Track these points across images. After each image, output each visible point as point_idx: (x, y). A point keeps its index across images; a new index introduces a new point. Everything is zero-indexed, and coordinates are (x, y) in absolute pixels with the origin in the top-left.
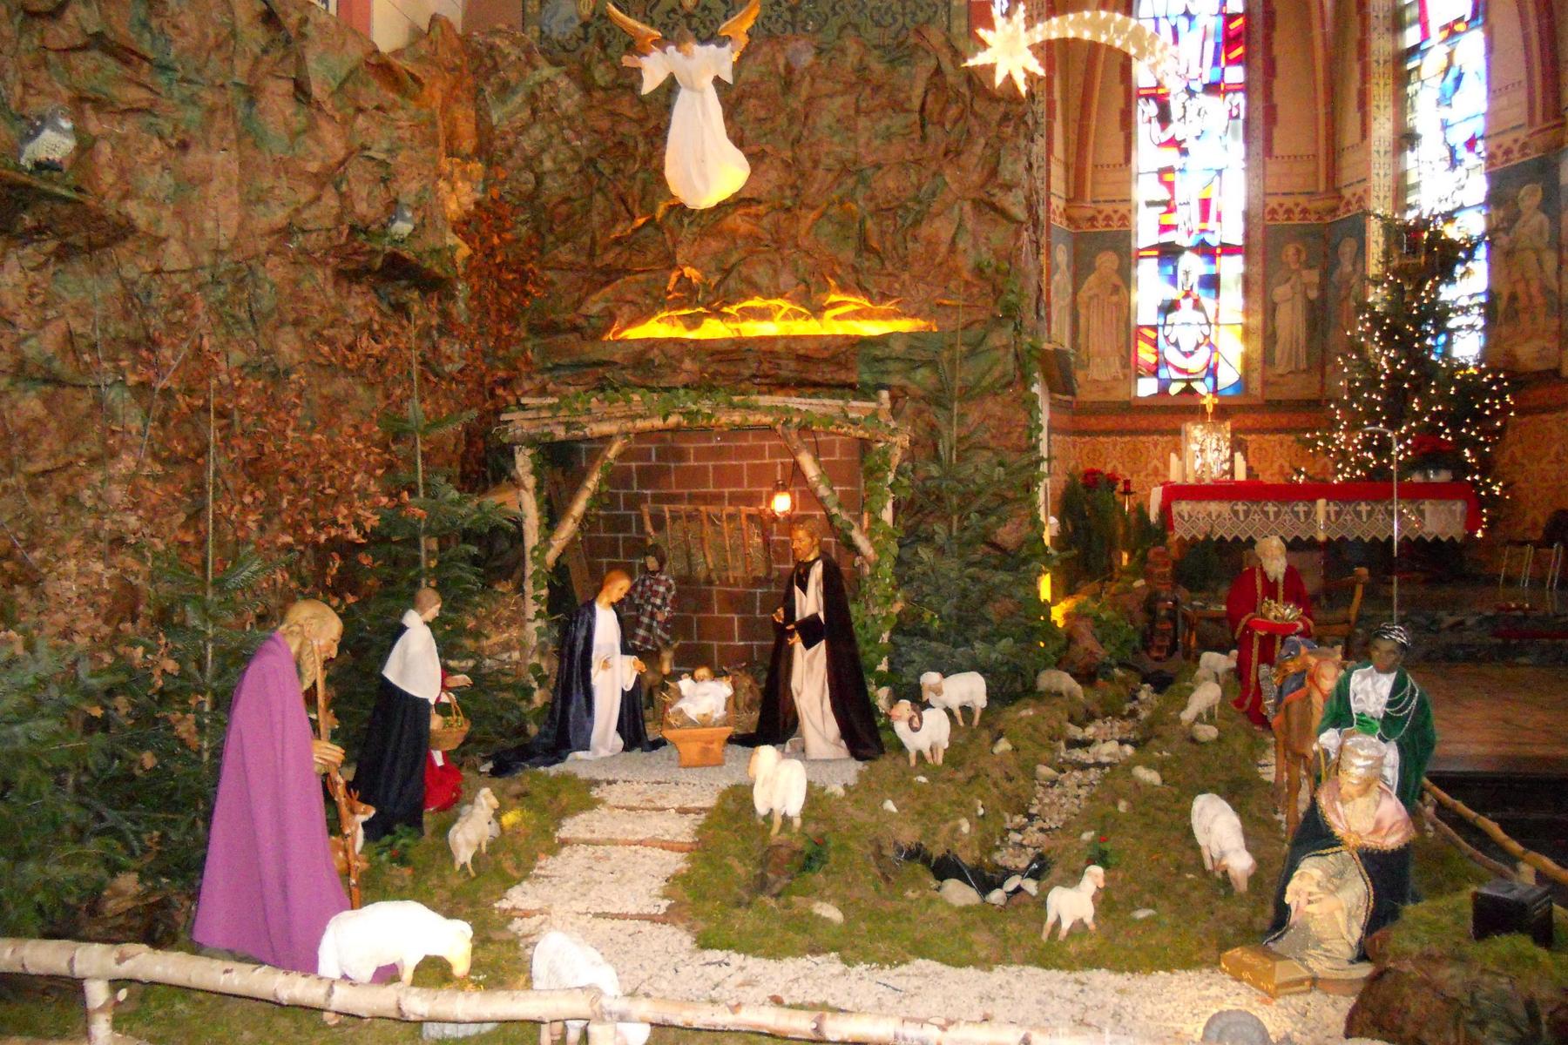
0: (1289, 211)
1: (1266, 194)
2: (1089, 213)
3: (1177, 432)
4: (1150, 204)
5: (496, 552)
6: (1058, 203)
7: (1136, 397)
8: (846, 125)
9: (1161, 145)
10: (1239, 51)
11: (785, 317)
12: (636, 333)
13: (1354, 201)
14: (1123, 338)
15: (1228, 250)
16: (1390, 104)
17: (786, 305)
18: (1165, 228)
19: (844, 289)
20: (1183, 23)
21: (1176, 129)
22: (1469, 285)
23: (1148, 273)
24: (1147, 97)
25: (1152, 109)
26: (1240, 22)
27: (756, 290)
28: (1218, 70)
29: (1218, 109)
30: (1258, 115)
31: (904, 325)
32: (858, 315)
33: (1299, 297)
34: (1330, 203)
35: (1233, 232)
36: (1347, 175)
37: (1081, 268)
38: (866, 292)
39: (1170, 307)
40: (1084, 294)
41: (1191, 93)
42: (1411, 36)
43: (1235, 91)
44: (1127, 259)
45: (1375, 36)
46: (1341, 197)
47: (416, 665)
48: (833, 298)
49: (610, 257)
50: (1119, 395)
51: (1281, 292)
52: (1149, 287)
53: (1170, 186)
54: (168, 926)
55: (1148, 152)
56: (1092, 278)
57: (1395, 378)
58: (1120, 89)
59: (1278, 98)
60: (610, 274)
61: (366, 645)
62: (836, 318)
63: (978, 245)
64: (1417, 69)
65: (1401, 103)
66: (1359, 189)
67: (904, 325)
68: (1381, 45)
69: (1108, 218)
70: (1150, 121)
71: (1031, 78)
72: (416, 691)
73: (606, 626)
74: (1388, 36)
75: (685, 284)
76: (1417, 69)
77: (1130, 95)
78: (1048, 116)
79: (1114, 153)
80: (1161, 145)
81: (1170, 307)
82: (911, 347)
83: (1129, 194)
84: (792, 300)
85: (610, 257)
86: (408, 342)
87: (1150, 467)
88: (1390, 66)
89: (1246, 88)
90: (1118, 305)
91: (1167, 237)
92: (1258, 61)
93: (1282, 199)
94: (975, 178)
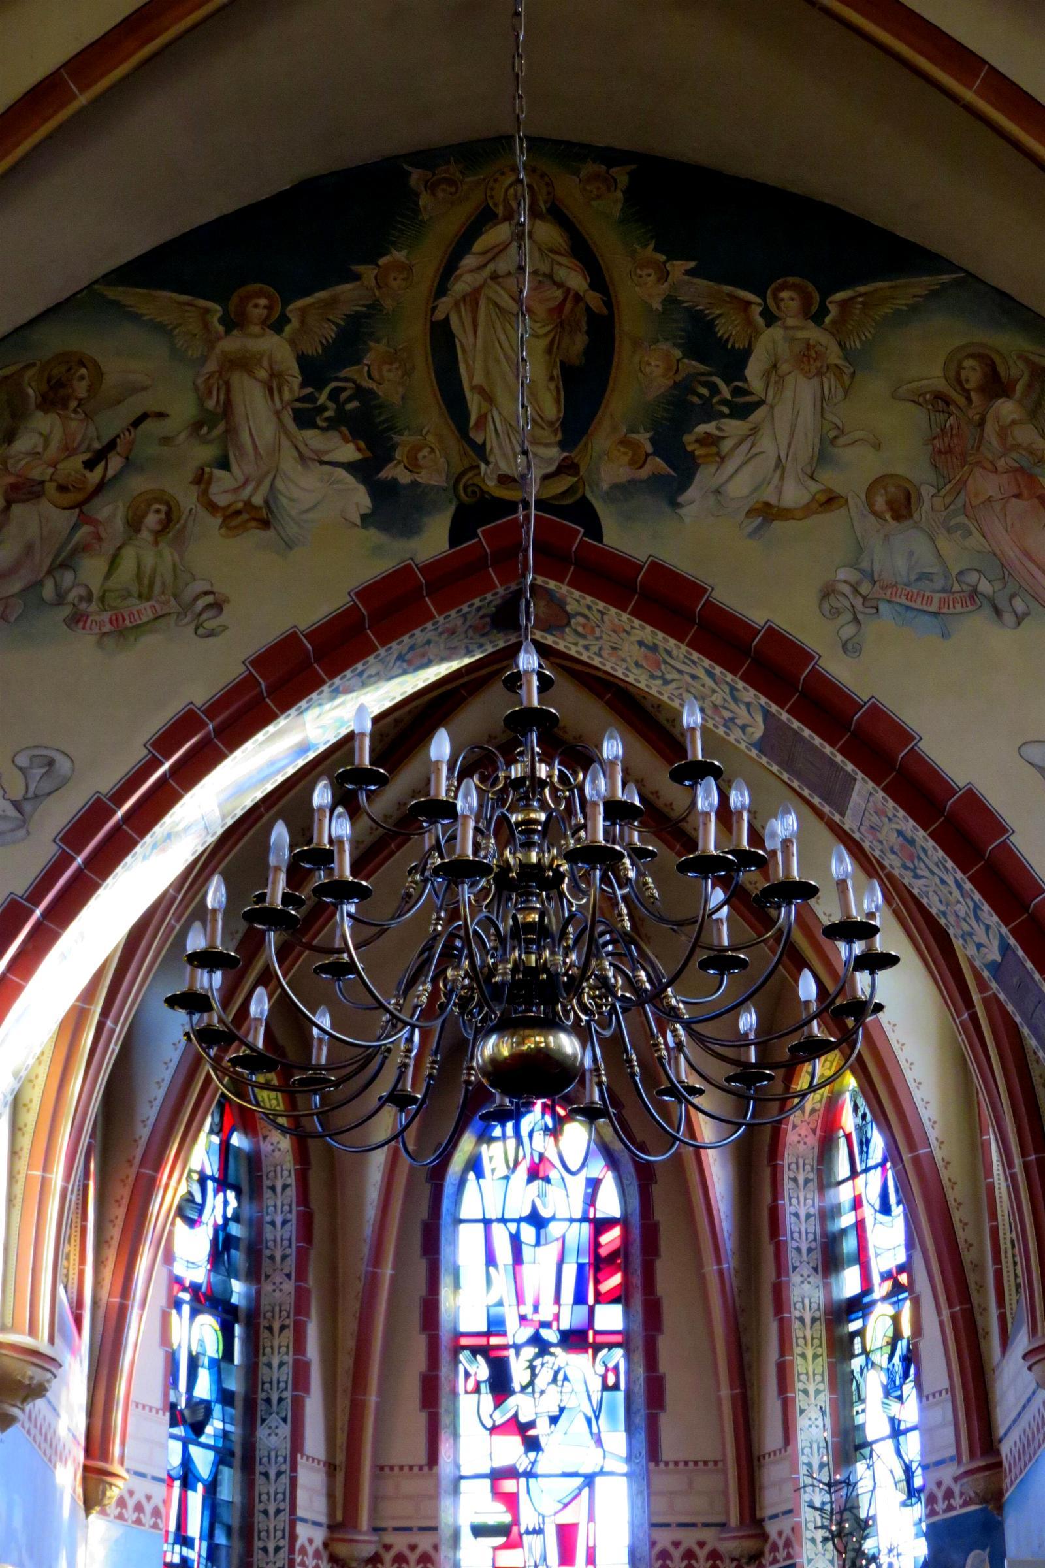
1: (654, 1525)
2: (367, 1551)
4: (479, 1531)
9: (494, 1430)
10: (616, 1280)
13: (781, 1544)
16: (824, 1387)
20: (528, 1233)
21: (521, 1405)
24: (475, 1351)
25: (481, 1370)
26: (616, 1232)
28: (583, 1310)
30: (640, 1389)
34: (750, 1545)
36: (772, 1500)
42: (849, 1283)
43: (611, 1346)
45: (795, 1278)
46: (764, 1536)
53: (511, 1501)
55: (475, 1440)
58: (420, 1343)
59: (664, 1366)
64: (860, 1333)
68: (806, 1293)
70: (477, 1390)
74: (816, 1280)
76: (860, 1333)
78: (296, 1387)
79: (407, 1445)
80: (494, 1430)
83: (436, 1516)
88: (820, 1327)
89: (624, 1340)
92: (637, 1300)
93: (679, 1534)
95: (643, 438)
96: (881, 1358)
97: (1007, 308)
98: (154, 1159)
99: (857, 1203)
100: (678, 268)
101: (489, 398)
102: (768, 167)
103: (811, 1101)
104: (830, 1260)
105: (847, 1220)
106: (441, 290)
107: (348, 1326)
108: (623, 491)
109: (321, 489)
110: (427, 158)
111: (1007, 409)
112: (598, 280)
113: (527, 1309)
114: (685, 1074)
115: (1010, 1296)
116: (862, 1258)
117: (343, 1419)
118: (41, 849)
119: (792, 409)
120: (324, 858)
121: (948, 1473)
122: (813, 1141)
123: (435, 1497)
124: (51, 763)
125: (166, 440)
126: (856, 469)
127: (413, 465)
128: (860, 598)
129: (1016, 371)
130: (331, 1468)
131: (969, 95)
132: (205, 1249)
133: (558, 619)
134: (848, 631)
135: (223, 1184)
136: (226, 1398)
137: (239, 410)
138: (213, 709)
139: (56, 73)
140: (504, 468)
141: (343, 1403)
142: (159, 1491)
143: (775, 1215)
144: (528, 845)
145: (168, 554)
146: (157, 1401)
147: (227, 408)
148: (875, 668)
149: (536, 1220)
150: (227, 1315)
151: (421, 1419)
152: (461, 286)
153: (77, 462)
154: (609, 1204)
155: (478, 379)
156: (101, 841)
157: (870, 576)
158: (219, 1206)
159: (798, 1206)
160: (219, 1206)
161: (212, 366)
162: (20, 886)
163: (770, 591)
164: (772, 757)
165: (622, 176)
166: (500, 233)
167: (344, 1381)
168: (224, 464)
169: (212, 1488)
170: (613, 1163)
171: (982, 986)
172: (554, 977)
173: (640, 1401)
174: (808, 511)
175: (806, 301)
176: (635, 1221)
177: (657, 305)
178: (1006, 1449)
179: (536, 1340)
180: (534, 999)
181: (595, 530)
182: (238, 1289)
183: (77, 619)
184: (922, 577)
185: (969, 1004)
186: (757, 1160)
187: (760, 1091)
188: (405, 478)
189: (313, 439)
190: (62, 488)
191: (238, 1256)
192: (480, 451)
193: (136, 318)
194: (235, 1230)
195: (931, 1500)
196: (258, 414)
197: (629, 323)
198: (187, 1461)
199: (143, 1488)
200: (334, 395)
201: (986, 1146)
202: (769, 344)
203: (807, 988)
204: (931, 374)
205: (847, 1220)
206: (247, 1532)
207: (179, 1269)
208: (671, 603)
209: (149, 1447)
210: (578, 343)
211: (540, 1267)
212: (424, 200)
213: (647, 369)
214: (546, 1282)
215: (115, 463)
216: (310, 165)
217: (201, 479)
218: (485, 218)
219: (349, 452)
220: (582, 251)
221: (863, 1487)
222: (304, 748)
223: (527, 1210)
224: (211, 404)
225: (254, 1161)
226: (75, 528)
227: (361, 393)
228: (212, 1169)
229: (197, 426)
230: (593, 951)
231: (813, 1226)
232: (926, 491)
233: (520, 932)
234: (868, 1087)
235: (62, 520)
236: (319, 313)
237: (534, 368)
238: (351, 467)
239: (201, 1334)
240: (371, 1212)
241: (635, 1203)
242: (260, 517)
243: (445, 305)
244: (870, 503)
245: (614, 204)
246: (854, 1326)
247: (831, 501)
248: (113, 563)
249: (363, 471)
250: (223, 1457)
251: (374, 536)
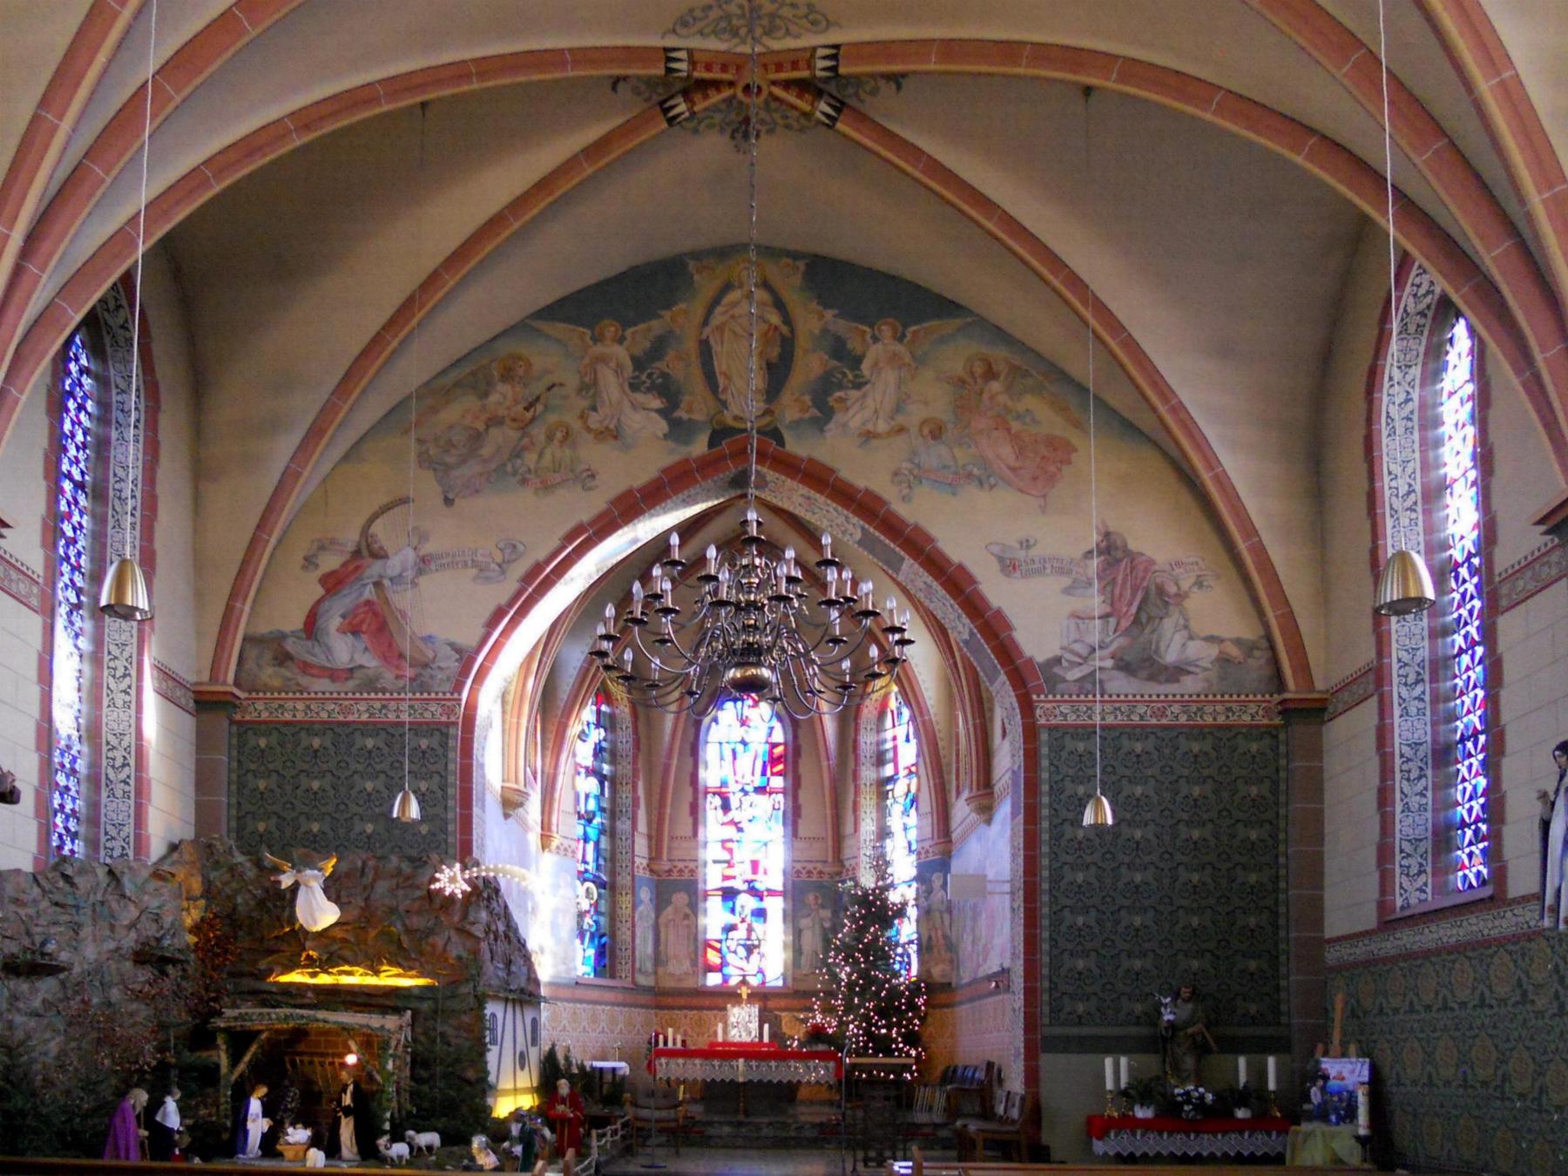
0: (809, 872)
3: (725, 1009)
5: (210, 1075)
6: (641, 861)
7: (704, 986)
10: (780, 767)
12: (284, 979)
14: (692, 948)
15: (772, 893)
17: (361, 970)
18: (726, 878)
20: (740, 748)
21: (734, 814)
22: (907, 930)
23: (715, 905)
25: (717, 801)
27: (348, 962)
29: (764, 802)
30: (790, 811)
31: (421, 982)
32: (398, 975)
33: (817, 927)
34: (837, 869)
35: (777, 883)
36: (847, 853)
37: (660, 902)
38: (400, 965)
39: (730, 928)
40: (662, 920)
41: (746, 793)
42: (888, 770)
44: (694, 895)
47: (171, 1115)
50: (689, 983)
51: (805, 922)
52: (714, 917)
53: (730, 851)
55: (714, 826)
56: (670, 909)
57: (851, 985)
58: (689, 792)
60: (271, 952)
61: (156, 1104)
63: (457, 949)
65: (882, 812)
66: (853, 862)
67: (421, 982)
68: (868, 774)
69: (681, 871)
71: (463, 892)
72: (169, 1125)
73: (255, 1106)
74: (873, 769)
75: (309, 957)
77: (697, 792)
79: (684, 827)
81: (730, 928)
86: (167, 985)
88: (874, 788)
89: (784, 791)
90: (688, 926)
91: (728, 884)
94: (456, 919)
95: (807, 398)
96: (901, 800)
97: (1000, 335)
98: (567, 714)
99: (894, 738)
100: (829, 314)
101: (728, 377)
102: (881, 263)
103: (874, 696)
104: (880, 760)
105: (889, 745)
106: (705, 323)
107: (657, 780)
108: (796, 424)
109: (644, 421)
110: (696, 255)
111: (995, 386)
112: (787, 320)
113: (739, 778)
114: (817, 686)
115: (962, 776)
116: (895, 760)
117: (655, 818)
118: (511, 585)
119: (883, 386)
120: (658, 597)
121: (927, 844)
122: (875, 713)
123: (696, 849)
124: (514, 547)
125: (565, 397)
126: (915, 414)
127: (690, 410)
128: (913, 476)
129: (1001, 367)
130: (650, 837)
131: (990, 225)
132: (591, 752)
133: (762, 483)
134: (906, 491)
135: (598, 725)
136: (602, 810)
137: (601, 382)
138: (592, 523)
139: (502, 211)
140: (737, 412)
141: (655, 812)
142: (574, 844)
143: (855, 741)
144: (750, 592)
145: (568, 452)
146: (571, 810)
147: (595, 383)
148: (921, 509)
149: (744, 743)
150: (602, 779)
151: (690, 820)
152: (718, 318)
153: (520, 408)
154: (778, 736)
155: (724, 367)
156: (539, 582)
157: (918, 466)
158: (597, 735)
159: (867, 740)
160: (597, 735)
161: (587, 361)
162: (503, 601)
163: (868, 472)
164: (865, 548)
165: (801, 265)
166: (734, 295)
167: (655, 804)
168: (594, 409)
169: (597, 844)
170: (780, 719)
171: (960, 650)
172: (760, 647)
173: (790, 815)
174: (889, 434)
175: (895, 330)
176: (790, 743)
177: (817, 332)
178: (954, 836)
179: (742, 790)
180: (752, 654)
181: (781, 441)
182: (606, 769)
183: (524, 481)
184: (945, 467)
185: (953, 657)
186: (849, 721)
187: (851, 692)
188: (685, 416)
189: (640, 397)
190: (514, 420)
191: (606, 755)
192: (724, 404)
193: (548, 337)
194: (604, 744)
195: (919, 854)
196: (611, 385)
197: (803, 341)
198: (585, 833)
199: (566, 843)
200: (650, 376)
201: (956, 718)
202: (874, 352)
203: (874, 652)
204: (957, 367)
205: (889, 745)
206: (613, 859)
207: (579, 760)
208: (818, 478)
209: (568, 827)
210: (775, 352)
211: (745, 761)
212: (696, 277)
213: (810, 364)
214: (748, 769)
215: (540, 407)
216: (639, 260)
217: (583, 417)
218: (727, 287)
219: (657, 403)
220: (780, 305)
221: (888, 849)
222: (635, 541)
223: (739, 737)
224: (587, 379)
225: (612, 717)
226: (521, 439)
227: (664, 375)
228: (593, 719)
229: (581, 390)
230: (779, 635)
231: (874, 747)
232: (950, 426)
233: (746, 628)
234: (903, 691)
235: (514, 435)
236: (641, 335)
237: (754, 363)
238: (658, 411)
239: (590, 785)
240: (667, 738)
241: (790, 737)
242: (612, 434)
243: (707, 331)
244: (921, 430)
245: (797, 280)
246: (889, 787)
247: (901, 430)
248: (541, 455)
249: (664, 413)
250: (602, 832)
251: (670, 444)
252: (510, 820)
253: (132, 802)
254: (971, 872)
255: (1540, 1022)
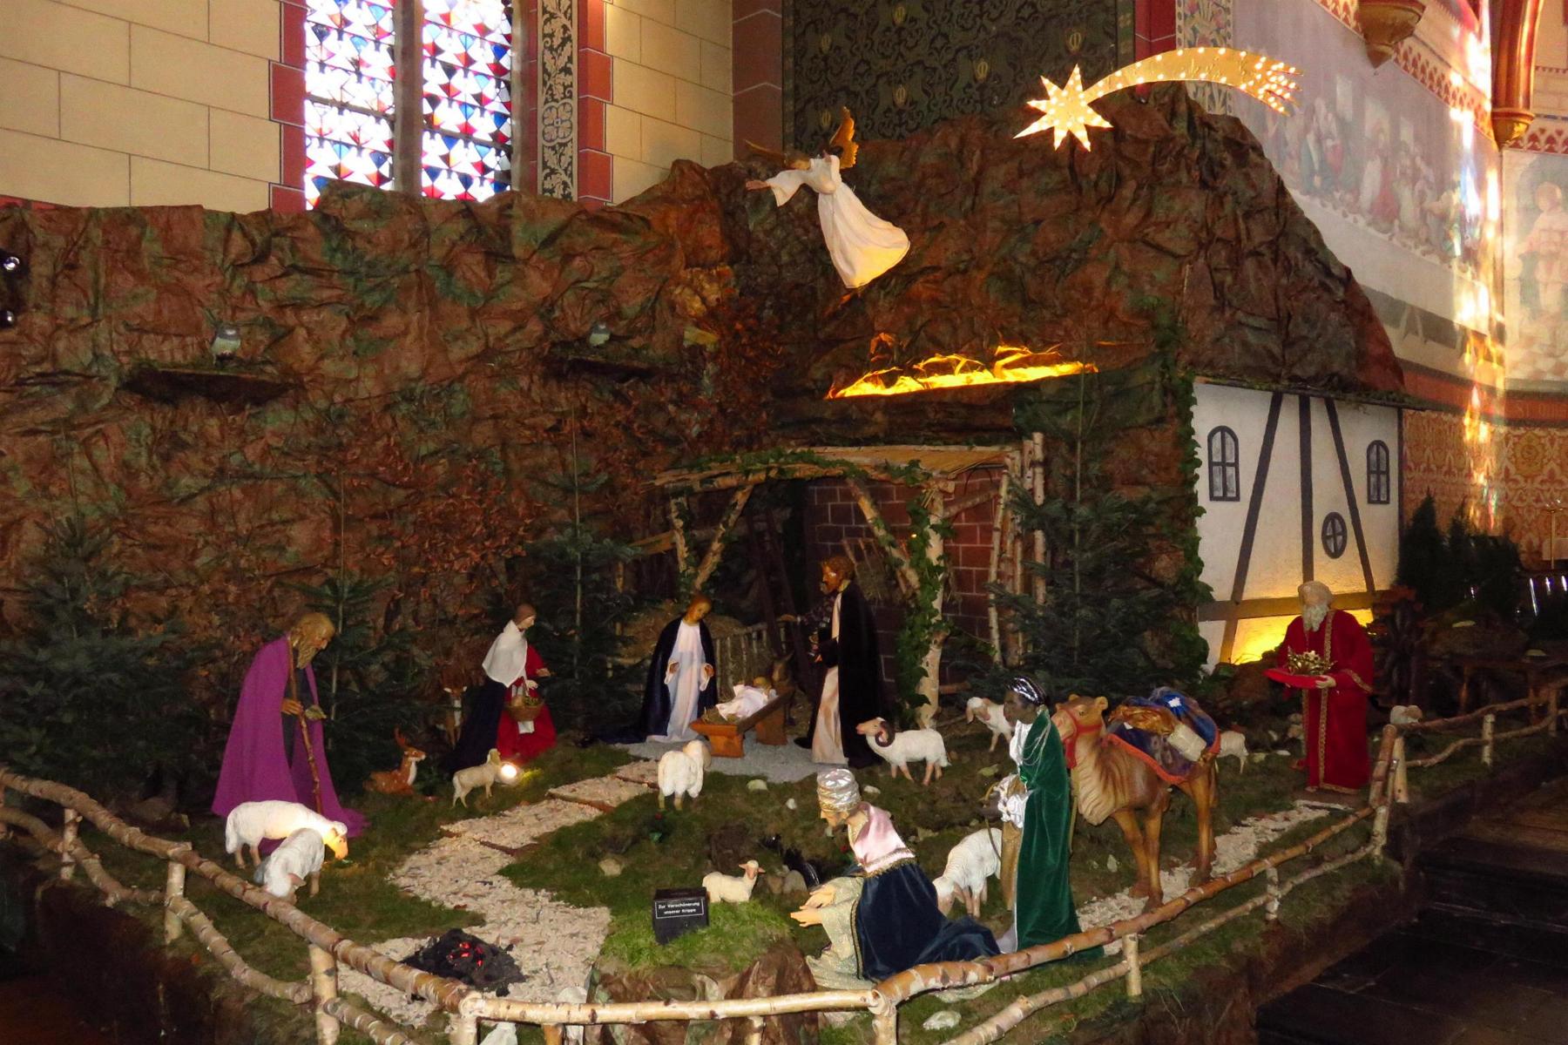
8: (1011, 186)
11: (963, 370)
12: (849, 392)
19: (1009, 340)
32: (1024, 363)
48: (1001, 349)
49: (829, 329)
54: (184, 829)
62: (1007, 366)
71: (1093, 132)
82: (1064, 390)
84: (967, 355)
85: (829, 329)
87: (1546, 470)
252: (1387, 67)
253: (574, 103)
254: (913, 971)
255: (1528, 486)
